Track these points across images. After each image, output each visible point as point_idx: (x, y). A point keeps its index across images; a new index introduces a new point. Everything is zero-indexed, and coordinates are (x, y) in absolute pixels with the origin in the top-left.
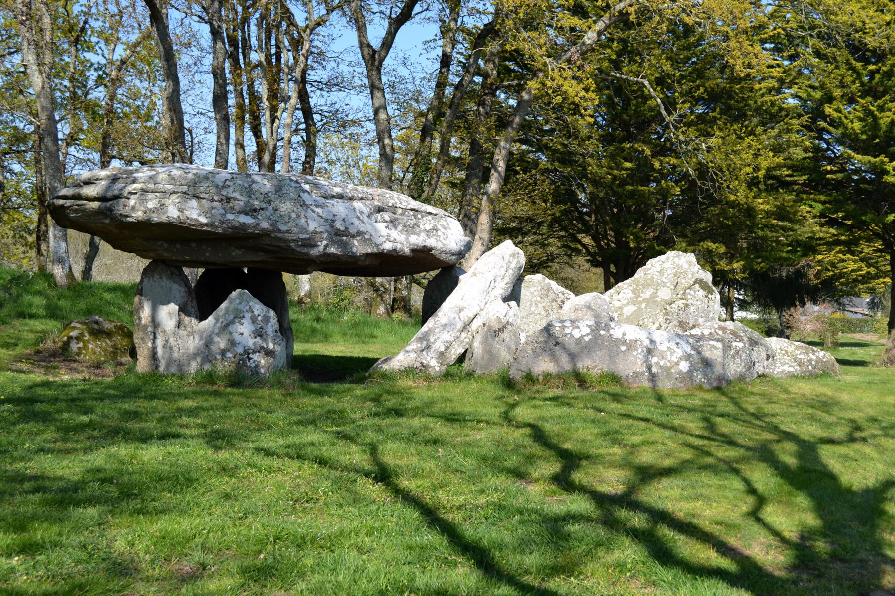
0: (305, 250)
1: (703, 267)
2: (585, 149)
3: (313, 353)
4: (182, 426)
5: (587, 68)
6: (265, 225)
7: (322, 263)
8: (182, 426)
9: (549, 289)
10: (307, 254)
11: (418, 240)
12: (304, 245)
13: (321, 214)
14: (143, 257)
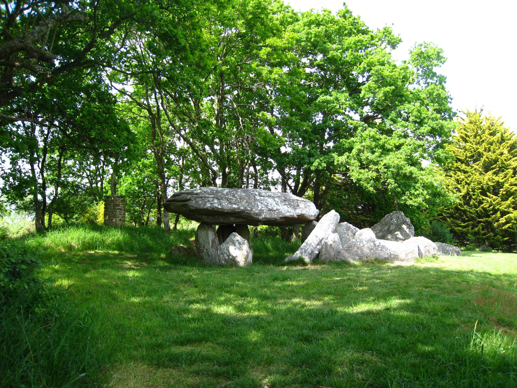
0: (257, 217)
1: (265, 218)
2: (108, 308)
3: (447, 269)
4: (383, 274)
5: (138, 177)
6: (242, 208)
7: (264, 221)
8: (383, 274)
9: (349, 227)
10: (258, 218)
11: (299, 212)
12: (257, 215)
13: (173, 220)
14: (198, 222)
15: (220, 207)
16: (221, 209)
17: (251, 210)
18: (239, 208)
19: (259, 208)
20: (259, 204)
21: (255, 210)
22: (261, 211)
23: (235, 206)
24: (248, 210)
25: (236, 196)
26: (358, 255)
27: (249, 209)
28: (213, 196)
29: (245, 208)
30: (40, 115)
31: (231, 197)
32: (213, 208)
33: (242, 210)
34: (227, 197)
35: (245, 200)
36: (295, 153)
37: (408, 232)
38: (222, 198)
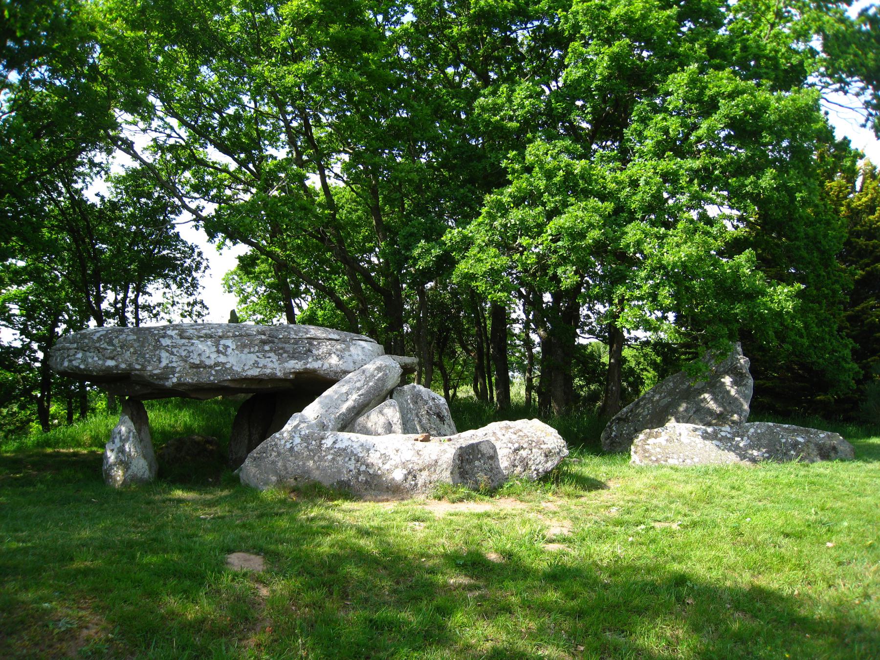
0: (162, 382)
6: (123, 366)
10: (164, 385)
12: (161, 379)
15: (82, 367)
16: (84, 369)
17: (144, 368)
18: (117, 366)
19: (163, 364)
20: (164, 354)
21: (152, 369)
22: (169, 370)
23: (111, 363)
24: (137, 370)
25: (116, 341)
26: (275, 473)
27: (138, 367)
28: (75, 345)
29: (130, 365)
30: (14, 238)
31: (105, 345)
32: (72, 369)
33: (123, 369)
34: (98, 345)
35: (132, 350)
36: (446, 244)
37: (733, 392)
38: (90, 348)
